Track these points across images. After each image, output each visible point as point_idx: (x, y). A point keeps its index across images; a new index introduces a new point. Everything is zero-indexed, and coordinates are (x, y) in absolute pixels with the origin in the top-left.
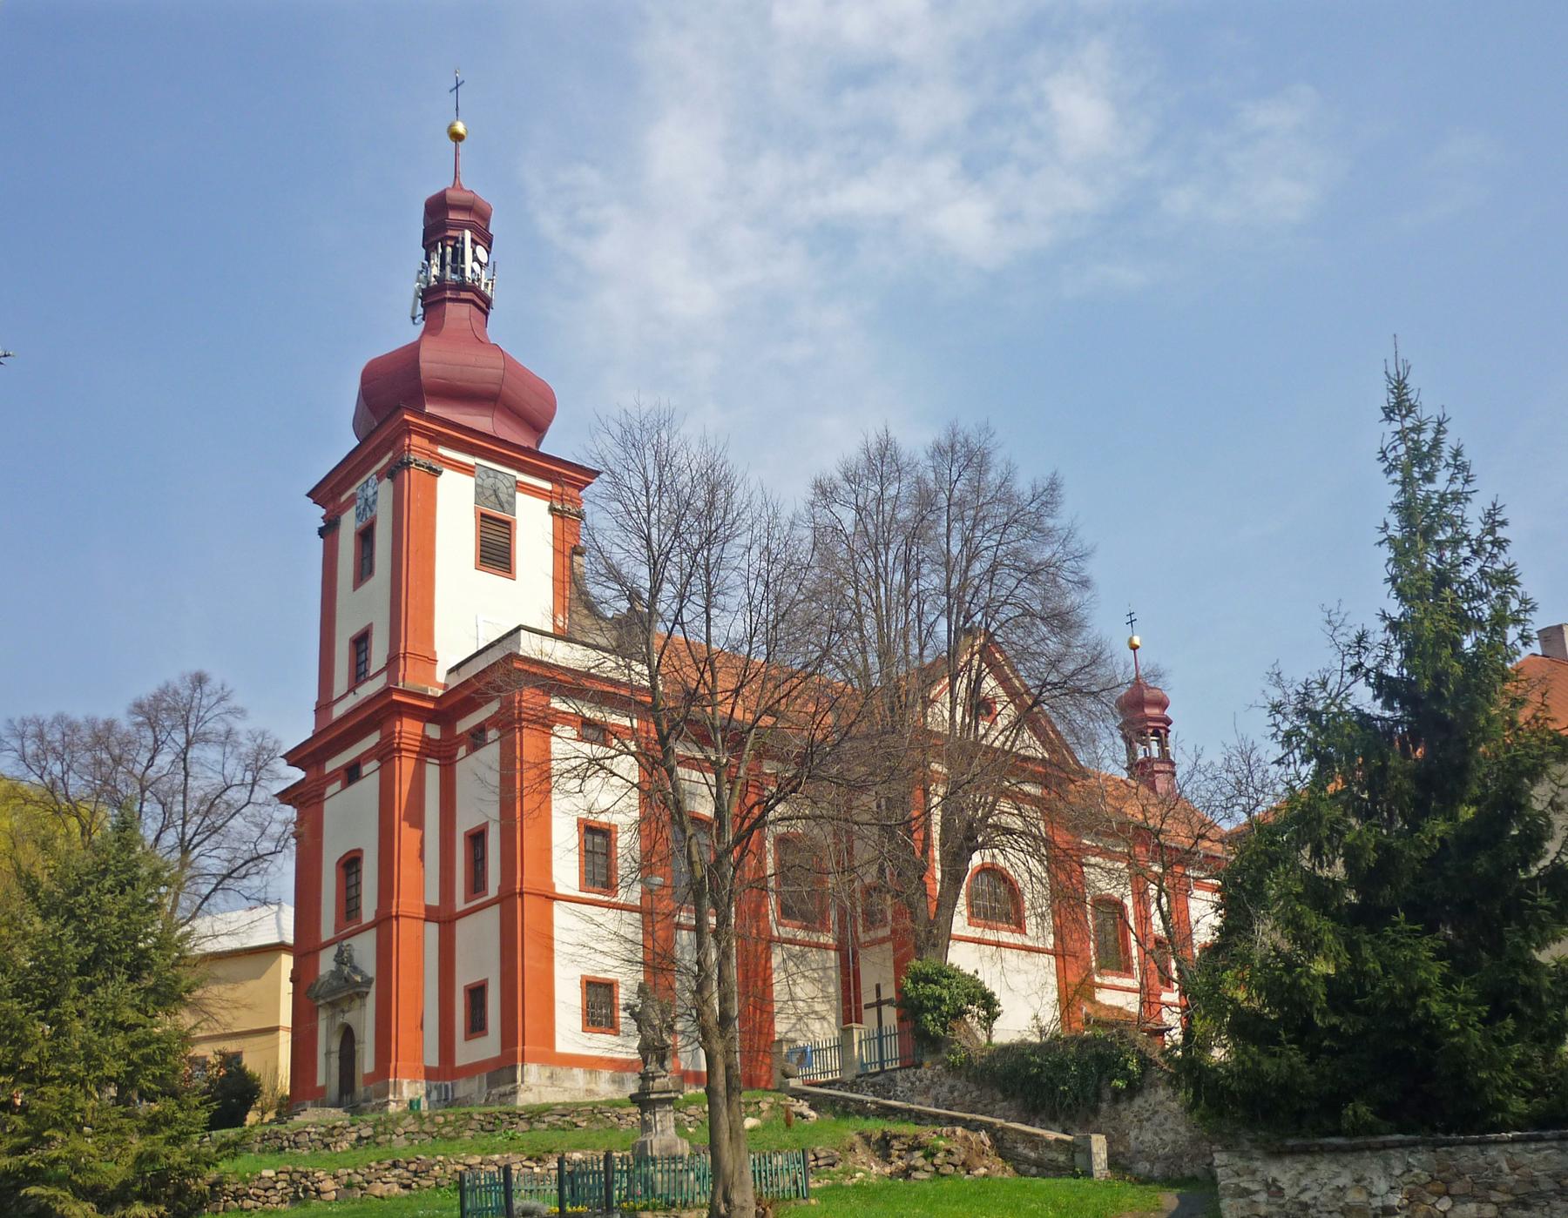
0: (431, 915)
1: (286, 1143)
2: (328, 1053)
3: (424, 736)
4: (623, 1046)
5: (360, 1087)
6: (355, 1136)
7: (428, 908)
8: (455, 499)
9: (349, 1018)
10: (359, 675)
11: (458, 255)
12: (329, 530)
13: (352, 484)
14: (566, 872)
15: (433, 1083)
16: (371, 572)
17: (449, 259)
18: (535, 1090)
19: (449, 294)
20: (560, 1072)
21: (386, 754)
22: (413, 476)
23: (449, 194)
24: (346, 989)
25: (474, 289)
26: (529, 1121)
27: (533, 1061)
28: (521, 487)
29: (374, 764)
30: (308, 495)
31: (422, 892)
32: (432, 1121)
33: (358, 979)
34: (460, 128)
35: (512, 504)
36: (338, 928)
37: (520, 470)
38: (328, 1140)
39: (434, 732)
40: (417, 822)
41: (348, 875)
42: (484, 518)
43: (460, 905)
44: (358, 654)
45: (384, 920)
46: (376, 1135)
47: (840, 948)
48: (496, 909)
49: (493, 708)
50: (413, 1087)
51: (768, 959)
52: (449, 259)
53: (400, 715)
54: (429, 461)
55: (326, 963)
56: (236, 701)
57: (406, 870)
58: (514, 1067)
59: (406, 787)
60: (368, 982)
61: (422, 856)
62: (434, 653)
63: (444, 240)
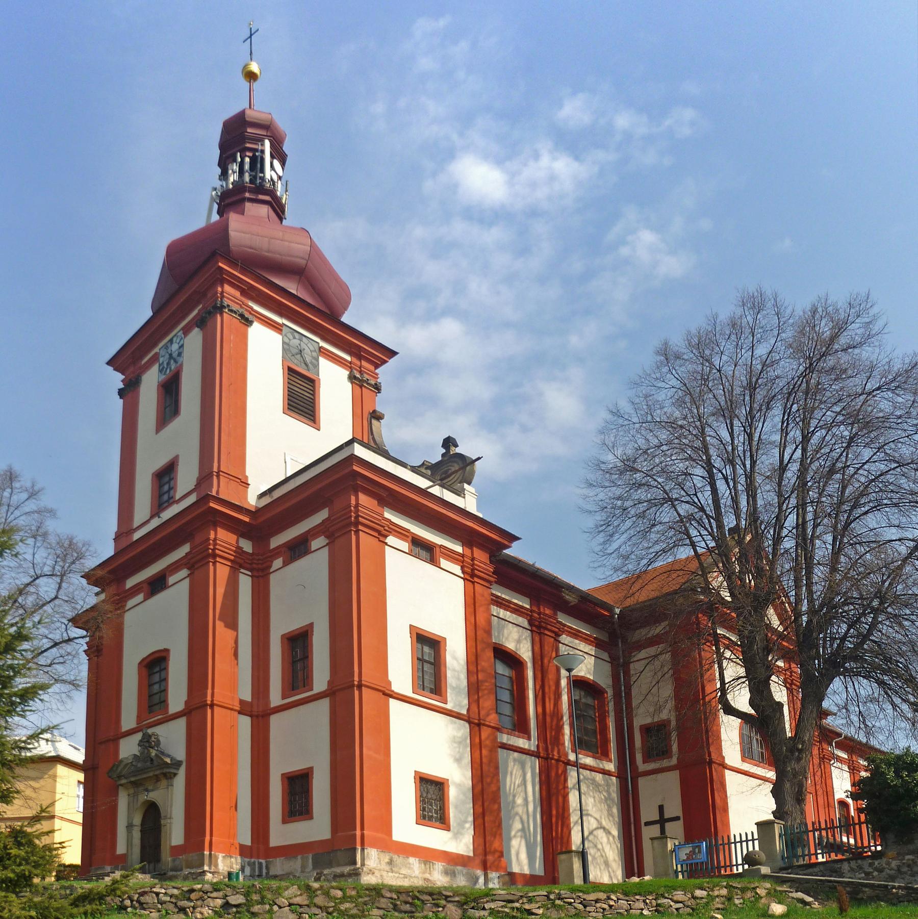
0: (244, 709)
1: (128, 903)
2: (130, 827)
3: (238, 548)
4: (459, 841)
5: (166, 857)
6: (219, 902)
7: (242, 702)
8: (264, 351)
9: (153, 796)
10: (161, 501)
11: (257, 163)
12: (129, 391)
13: (155, 345)
14: (400, 671)
15: (247, 860)
16: (176, 412)
17: (247, 167)
18: (377, 873)
19: (247, 195)
20: (398, 860)
21: (198, 563)
22: (226, 322)
23: (248, 113)
24: (153, 768)
25: (272, 193)
26: (461, 905)
27: (373, 846)
28: (322, 352)
29: (184, 573)
30: (109, 363)
31: (234, 684)
32: (327, 894)
33: (168, 760)
34: (254, 67)
35: (316, 366)
36: (139, 718)
37: (324, 339)
38: (184, 903)
39: (247, 546)
40: (232, 624)
41: (150, 675)
42: (291, 372)
43: (275, 698)
44: (161, 486)
45: (197, 710)
46: (249, 903)
47: (621, 775)
48: (325, 704)
49: (323, 515)
50: (228, 861)
51: (566, 780)
52: (247, 167)
53: (215, 525)
54: (241, 310)
55: (129, 748)
56: (46, 501)
57: (220, 665)
58: (354, 850)
59: (221, 591)
60: (178, 764)
61: (236, 655)
62: (247, 477)
63: (243, 151)
